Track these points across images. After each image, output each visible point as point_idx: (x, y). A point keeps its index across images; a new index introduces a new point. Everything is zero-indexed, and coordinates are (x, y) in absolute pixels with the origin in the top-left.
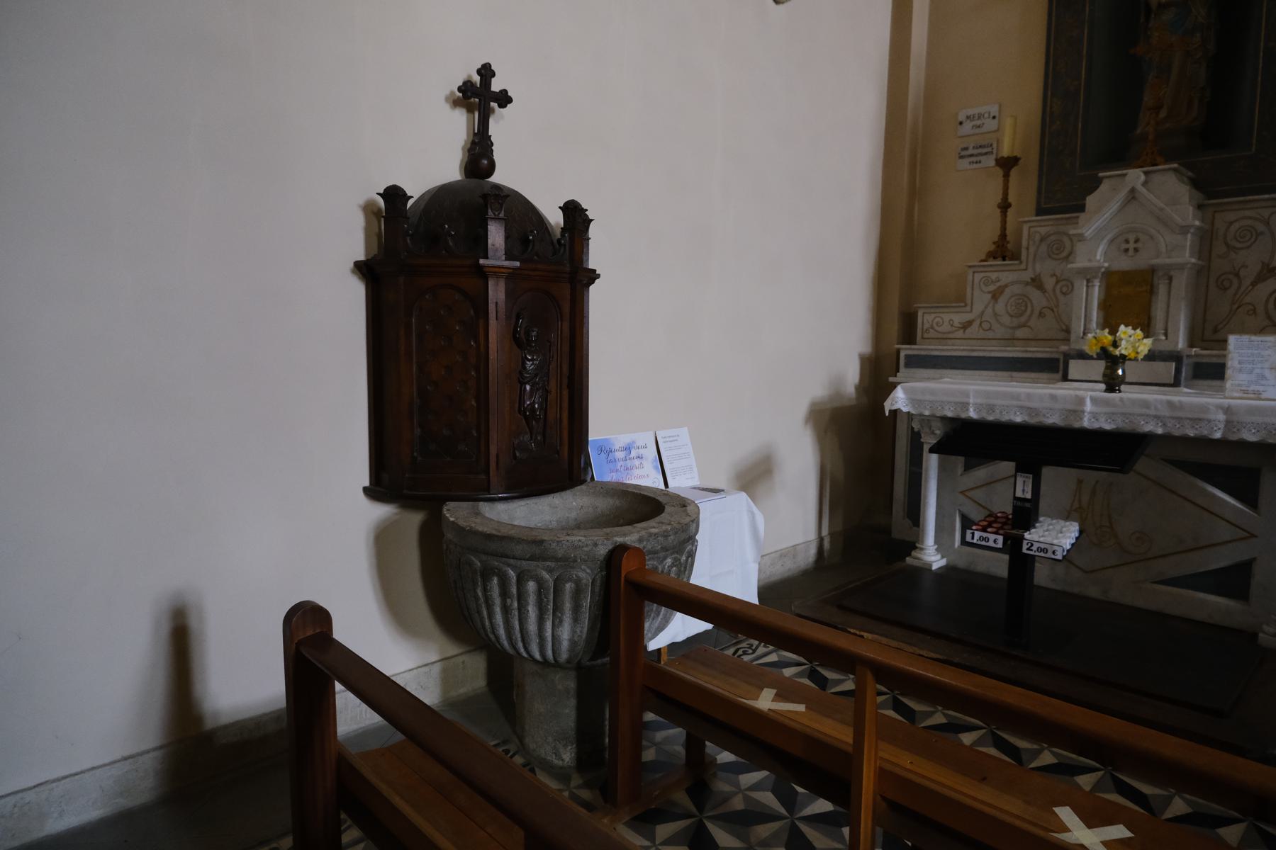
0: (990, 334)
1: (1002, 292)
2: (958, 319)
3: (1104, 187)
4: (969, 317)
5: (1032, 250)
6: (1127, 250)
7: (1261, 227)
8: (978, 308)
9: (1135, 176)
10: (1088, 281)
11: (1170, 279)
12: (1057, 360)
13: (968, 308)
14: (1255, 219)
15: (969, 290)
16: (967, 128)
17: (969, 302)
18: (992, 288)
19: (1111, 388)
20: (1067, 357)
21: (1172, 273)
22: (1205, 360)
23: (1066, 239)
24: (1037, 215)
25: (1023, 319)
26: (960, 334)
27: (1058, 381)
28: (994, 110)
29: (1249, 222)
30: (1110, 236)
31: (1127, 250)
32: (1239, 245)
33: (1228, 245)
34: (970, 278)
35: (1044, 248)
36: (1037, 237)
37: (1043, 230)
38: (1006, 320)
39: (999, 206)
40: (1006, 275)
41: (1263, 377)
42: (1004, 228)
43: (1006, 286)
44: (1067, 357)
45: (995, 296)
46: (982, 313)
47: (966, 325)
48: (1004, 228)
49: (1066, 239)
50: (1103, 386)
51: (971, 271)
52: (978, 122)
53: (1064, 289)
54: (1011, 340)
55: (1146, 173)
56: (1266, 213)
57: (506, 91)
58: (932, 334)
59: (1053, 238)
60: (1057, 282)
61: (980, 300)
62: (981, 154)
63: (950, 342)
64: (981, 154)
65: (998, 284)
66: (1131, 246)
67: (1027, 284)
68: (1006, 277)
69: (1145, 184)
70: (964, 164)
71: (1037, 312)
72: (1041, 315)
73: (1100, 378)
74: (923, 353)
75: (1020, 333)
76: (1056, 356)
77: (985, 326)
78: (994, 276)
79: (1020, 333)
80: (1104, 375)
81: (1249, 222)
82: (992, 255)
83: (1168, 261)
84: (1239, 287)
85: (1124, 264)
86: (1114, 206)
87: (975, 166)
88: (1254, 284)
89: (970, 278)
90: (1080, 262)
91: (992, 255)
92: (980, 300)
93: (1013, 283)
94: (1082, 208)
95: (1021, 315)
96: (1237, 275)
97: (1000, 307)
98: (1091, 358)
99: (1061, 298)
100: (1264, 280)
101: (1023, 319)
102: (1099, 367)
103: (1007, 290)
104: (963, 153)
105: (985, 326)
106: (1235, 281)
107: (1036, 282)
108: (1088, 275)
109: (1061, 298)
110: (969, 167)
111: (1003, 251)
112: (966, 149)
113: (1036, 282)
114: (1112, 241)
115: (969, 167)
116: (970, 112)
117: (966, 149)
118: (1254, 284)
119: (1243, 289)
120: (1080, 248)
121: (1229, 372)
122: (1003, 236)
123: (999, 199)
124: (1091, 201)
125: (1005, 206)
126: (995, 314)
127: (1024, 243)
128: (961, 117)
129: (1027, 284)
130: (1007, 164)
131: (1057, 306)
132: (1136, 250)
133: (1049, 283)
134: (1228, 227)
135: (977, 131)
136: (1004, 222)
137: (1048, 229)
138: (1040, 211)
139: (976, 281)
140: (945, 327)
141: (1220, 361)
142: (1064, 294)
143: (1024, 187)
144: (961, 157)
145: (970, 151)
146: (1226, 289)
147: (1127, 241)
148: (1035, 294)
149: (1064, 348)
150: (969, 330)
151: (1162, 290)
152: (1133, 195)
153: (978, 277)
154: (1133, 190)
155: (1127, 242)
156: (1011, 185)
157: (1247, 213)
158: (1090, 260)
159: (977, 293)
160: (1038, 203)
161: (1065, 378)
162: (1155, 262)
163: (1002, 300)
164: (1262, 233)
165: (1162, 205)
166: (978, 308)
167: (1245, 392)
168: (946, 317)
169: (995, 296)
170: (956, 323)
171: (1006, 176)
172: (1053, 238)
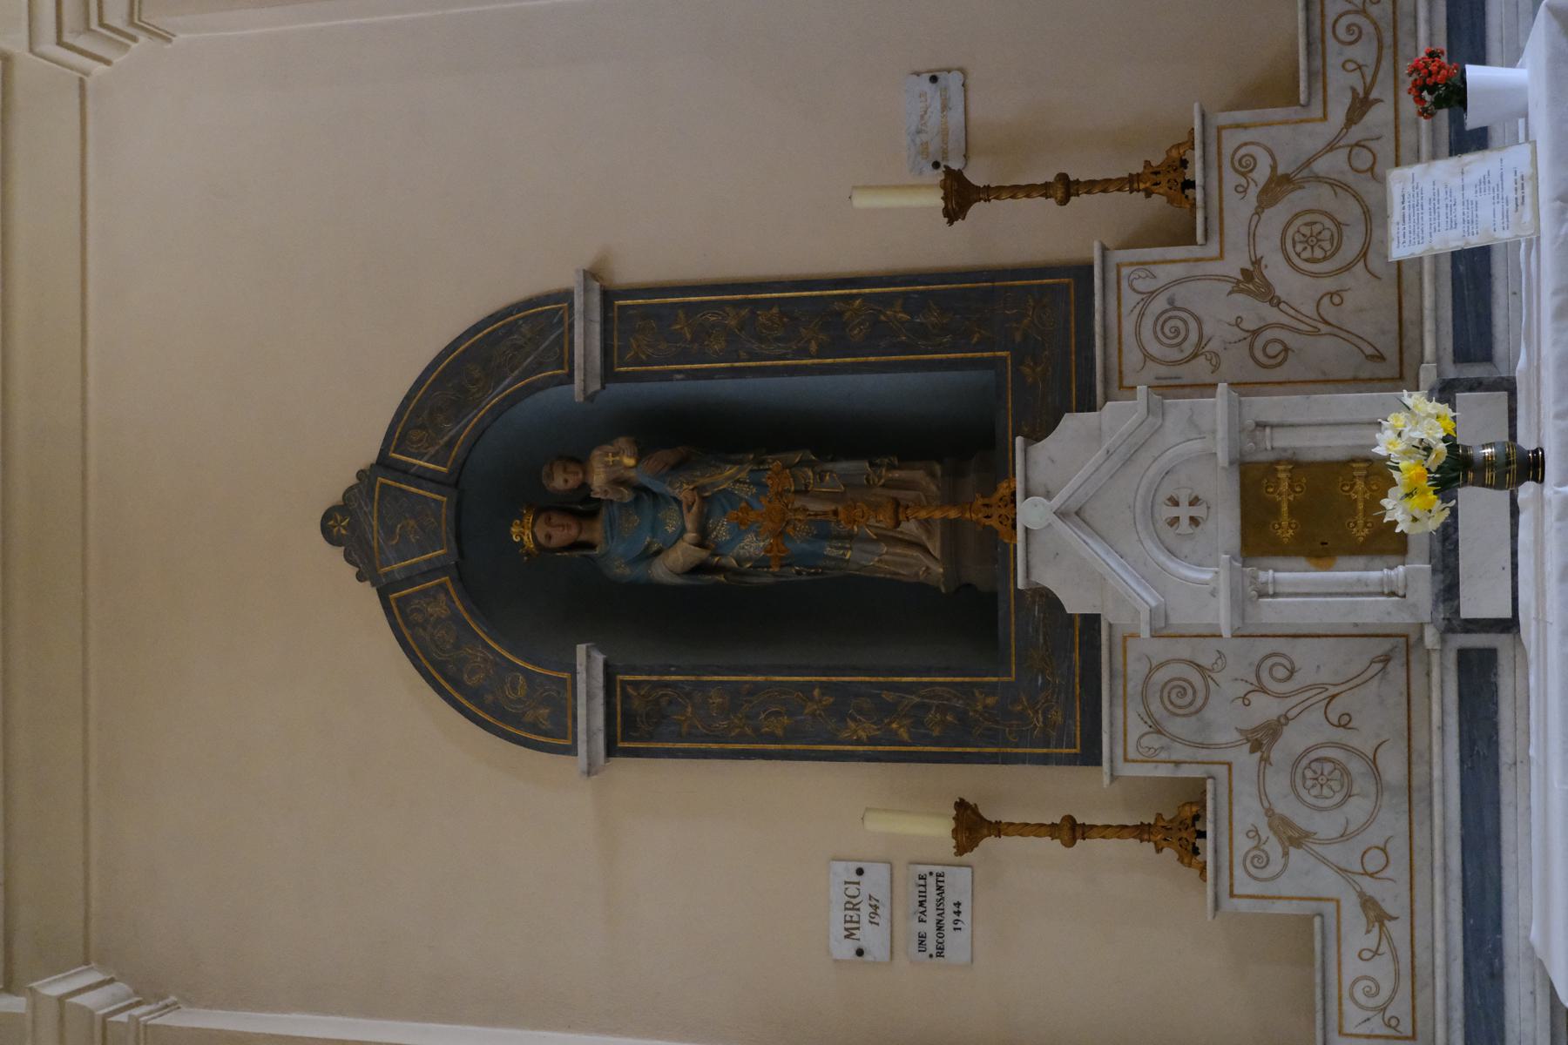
0: (1399, 848)
1: (1286, 822)
2: (1357, 935)
3: (1048, 577)
4: (1351, 907)
5: (1181, 752)
6: (1194, 521)
7: (1159, 304)
8: (1328, 883)
9: (1030, 513)
10: (1262, 595)
11: (1261, 426)
12: (1463, 654)
13: (1329, 908)
14: (1141, 315)
15: (1280, 908)
16: (872, 937)
17: (1307, 908)
18: (1274, 847)
19: (1532, 467)
20: (1455, 624)
21: (1250, 422)
22: (1448, 344)
23: (1160, 677)
24: (1099, 763)
25: (1356, 766)
26: (1398, 930)
27: (1518, 641)
28: (845, 871)
29: (1148, 323)
30: (1163, 558)
31: (1194, 521)
32: (1194, 337)
33: (1195, 356)
34: (1243, 905)
35: (1176, 726)
36: (1153, 741)
37: (1136, 728)
38: (1358, 809)
39: (1070, 843)
40: (1239, 817)
41: (1484, 181)
42: (1121, 831)
43: (1270, 812)
44: (1455, 624)
45: (1295, 838)
46: (1342, 871)
47: (1376, 914)
48: (1121, 831)
49: (1160, 677)
50: (1527, 491)
51: (1227, 904)
52: (865, 910)
53: (1281, 673)
54: (1413, 794)
55: (1027, 495)
56: (1130, 299)
57: (343, 525)
58: (1400, 1008)
59: (1155, 706)
60: (1263, 690)
61: (1306, 878)
62: (940, 902)
63: (1422, 957)
64: (940, 902)
65: (1265, 832)
66: (1184, 512)
67: (1265, 760)
68: (1248, 812)
69: (1048, 495)
70: (957, 943)
71: (1340, 735)
72: (1345, 723)
73: (1504, 496)
74: (1458, 1014)
75: (1392, 768)
76: (1452, 658)
77: (1374, 861)
78: (1243, 844)
79: (1392, 768)
80: (1499, 485)
81: (1148, 323)
82: (1191, 853)
83: (1222, 432)
84: (1282, 326)
85: (1225, 523)
86: (1095, 551)
87: (965, 916)
88: (1275, 302)
89: (1243, 905)
90: (1221, 615)
91: (1191, 853)
92: (1306, 878)
93: (1262, 794)
94: (1092, 622)
95: (1345, 772)
96: (1255, 333)
97: (1324, 825)
98: (1454, 512)
99: (1300, 680)
100: (1268, 285)
101: (1356, 766)
102: (1479, 505)
103: (1281, 808)
104: (931, 946)
105: (1374, 861)
106: (1269, 334)
107: (1262, 739)
108: (1247, 597)
109: (1300, 680)
110: (965, 934)
111: (1180, 828)
112: (922, 938)
113: (1262, 739)
114: (1172, 553)
115: (965, 934)
116: (838, 929)
117: (922, 938)
118: (1275, 302)
119: (1285, 320)
120: (1184, 616)
121: (1475, 241)
122: (1141, 831)
123: (1051, 847)
124: (1075, 603)
125: (1071, 831)
126: (1344, 836)
127: (1164, 771)
128: (846, 950)
129: (1265, 760)
130: (971, 826)
131: (1323, 687)
132: (1194, 502)
133: (1265, 709)
134: (1154, 359)
135: (884, 911)
136: (1107, 831)
137: (1133, 717)
138: (1090, 755)
139: (1254, 888)
140: (1382, 970)
141: (1446, 267)
142: (1292, 672)
143: (1024, 790)
144: (940, 952)
145: (930, 928)
146: (1286, 349)
147: (1174, 521)
148: (1294, 740)
149: (1431, 638)
150: (1389, 907)
151: (1285, 441)
152: (1073, 514)
153: (1244, 885)
154: (1062, 514)
155: (1178, 517)
156: (1017, 819)
157: (1128, 326)
158: (1214, 593)
159: (1284, 886)
160: (1071, 761)
161: (1509, 625)
162: (1223, 459)
163: (1302, 818)
164: (1171, 301)
165: (1101, 452)
166: (1328, 883)
167: (1519, 203)
168: (1353, 967)
169: (1295, 838)
170: (1371, 941)
171: (998, 829)
172: (1155, 706)
